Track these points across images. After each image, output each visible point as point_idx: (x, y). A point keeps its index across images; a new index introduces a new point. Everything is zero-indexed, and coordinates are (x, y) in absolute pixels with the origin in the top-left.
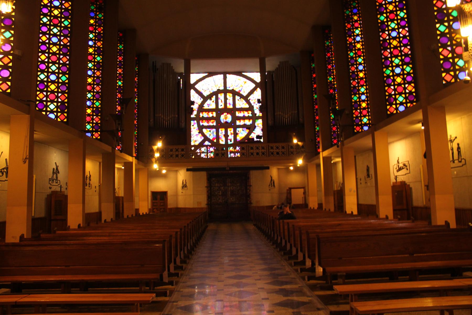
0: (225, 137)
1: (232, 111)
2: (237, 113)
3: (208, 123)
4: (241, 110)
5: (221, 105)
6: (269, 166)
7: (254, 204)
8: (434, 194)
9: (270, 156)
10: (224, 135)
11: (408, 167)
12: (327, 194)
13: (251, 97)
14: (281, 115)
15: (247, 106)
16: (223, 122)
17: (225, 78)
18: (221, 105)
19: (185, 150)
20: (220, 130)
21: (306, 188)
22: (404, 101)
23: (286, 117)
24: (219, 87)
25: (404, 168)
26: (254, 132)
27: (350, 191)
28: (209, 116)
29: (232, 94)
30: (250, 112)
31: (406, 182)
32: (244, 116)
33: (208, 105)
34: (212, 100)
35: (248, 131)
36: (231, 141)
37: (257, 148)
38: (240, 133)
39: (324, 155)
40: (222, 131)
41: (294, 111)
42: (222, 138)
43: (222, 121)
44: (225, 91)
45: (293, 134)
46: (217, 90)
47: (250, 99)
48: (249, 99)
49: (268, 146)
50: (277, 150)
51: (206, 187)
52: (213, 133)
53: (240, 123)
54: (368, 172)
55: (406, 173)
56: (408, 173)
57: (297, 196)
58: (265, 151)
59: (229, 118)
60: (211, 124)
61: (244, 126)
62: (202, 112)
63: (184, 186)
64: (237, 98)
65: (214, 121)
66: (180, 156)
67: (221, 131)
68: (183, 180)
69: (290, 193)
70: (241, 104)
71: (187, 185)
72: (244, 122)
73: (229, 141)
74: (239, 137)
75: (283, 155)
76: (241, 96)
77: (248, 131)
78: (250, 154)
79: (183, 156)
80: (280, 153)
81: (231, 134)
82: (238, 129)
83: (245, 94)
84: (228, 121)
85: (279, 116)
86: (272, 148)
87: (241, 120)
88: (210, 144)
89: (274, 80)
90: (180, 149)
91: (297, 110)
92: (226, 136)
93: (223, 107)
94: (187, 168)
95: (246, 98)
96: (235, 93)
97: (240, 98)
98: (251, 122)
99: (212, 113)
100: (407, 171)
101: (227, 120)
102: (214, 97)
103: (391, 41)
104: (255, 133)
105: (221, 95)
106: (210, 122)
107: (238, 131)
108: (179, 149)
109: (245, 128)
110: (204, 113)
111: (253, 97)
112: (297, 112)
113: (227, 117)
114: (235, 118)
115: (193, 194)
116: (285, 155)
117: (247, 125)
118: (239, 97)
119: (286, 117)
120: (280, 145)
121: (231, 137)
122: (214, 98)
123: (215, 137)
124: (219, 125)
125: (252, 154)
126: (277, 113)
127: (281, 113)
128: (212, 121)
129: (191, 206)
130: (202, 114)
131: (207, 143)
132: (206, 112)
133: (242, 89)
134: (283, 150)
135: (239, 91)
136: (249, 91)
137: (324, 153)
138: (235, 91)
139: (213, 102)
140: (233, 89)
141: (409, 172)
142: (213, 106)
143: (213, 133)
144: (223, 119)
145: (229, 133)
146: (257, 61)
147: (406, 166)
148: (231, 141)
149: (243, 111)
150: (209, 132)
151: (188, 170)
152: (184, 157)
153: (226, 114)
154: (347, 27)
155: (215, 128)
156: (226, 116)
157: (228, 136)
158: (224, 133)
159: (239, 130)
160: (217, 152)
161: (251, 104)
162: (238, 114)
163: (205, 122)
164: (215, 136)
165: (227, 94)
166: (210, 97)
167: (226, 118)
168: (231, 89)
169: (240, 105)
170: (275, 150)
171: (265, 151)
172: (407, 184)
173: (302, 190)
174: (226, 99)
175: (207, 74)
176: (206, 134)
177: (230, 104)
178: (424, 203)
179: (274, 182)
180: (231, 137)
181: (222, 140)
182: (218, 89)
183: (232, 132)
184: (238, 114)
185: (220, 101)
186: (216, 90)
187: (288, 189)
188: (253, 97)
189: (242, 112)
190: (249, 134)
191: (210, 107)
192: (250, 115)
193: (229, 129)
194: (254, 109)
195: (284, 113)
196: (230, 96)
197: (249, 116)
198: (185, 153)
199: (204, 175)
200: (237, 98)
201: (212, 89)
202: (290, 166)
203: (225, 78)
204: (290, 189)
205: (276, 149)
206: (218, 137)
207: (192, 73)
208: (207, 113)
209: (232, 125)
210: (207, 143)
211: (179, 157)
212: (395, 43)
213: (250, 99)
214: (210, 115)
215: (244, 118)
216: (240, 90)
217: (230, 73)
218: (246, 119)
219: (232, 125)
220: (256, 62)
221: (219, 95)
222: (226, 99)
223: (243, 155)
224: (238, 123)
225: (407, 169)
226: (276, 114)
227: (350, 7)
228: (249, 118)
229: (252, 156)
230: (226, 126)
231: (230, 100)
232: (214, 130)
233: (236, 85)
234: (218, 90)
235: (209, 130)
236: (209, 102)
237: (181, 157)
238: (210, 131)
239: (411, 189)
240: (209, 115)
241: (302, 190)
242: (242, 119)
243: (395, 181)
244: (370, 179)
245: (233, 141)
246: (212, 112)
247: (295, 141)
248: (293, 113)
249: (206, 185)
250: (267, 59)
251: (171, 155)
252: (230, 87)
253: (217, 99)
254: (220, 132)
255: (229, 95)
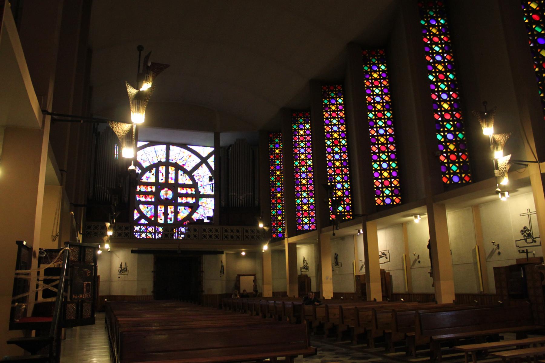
0: (164, 215)
1: (174, 187)
2: (179, 189)
3: (146, 198)
4: (184, 186)
5: (162, 180)
6: (223, 251)
7: (206, 292)
8: (439, 280)
9: (224, 239)
10: (164, 213)
11: (388, 256)
12: (291, 282)
13: (195, 173)
14: (235, 195)
15: (190, 182)
16: (163, 199)
17: (168, 150)
18: (162, 180)
19: (129, 229)
20: (159, 207)
21: (259, 276)
22: (390, 194)
23: (241, 199)
24: (161, 159)
25: (383, 257)
26: (197, 211)
27: (327, 279)
28: (147, 190)
29: (175, 168)
30: (193, 190)
31: (385, 270)
32: (187, 193)
33: (147, 177)
34: (152, 173)
35: (190, 210)
36: (171, 220)
37: (211, 230)
38: (181, 212)
39: (290, 242)
40: (162, 208)
41: (250, 193)
42: (161, 217)
43: (162, 198)
44: (167, 164)
45: (259, 218)
46: (159, 161)
47: (194, 175)
48: (193, 174)
49: (223, 228)
50: (232, 234)
51: (152, 272)
52: (151, 210)
53: (182, 201)
54: (337, 261)
55: (385, 261)
56: (388, 262)
57: (247, 284)
58: (219, 234)
59: (170, 195)
60: (149, 200)
61: (186, 205)
62: (140, 186)
63: (123, 270)
64: (180, 172)
65: (152, 196)
66: (123, 235)
67: (161, 208)
68: (122, 263)
69: (239, 281)
70: (184, 179)
71: (128, 269)
72: (187, 200)
73: (169, 220)
74: (181, 216)
75: (238, 239)
76: (185, 171)
77: (190, 210)
78: (202, 237)
79: (126, 235)
80: (235, 237)
81: (172, 212)
82: (179, 207)
83: (189, 169)
84: (168, 198)
85: (233, 197)
86: (226, 231)
87: (184, 198)
88: (146, 222)
89: (229, 157)
90: (123, 227)
91: (252, 191)
92: (166, 214)
93: (163, 181)
94: (131, 249)
95: (190, 173)
96: (178, 167)
97: (183, 173)
98: (194, 200)
99: (151, 188)
100: (387, 260)
101: (168, 196)
102: (154, 169)
103: (379, 138)
104: (198, 213)
105: (162, 167)
106: (148, 197)
107: (180, 210)
108: (98, 226)
109: (187, 206)
110: (142, 186)
111: (198, 173)
112: (252, 193)
113: (168, 193)
114: (177, 195)
115: (138, 280)
116: (240, 239)
117: (189, 203)
118: (182, 172)
119: (241, 199)
120: (235, 228)
121: (171, 216)
122: (154, 171)
123: (153, 215)
124: (159, 202)
125: (205, 236)
126: (231, 194)
127: (236, 194)
128: (150, 196)
129: (134, 294)
130: (140, 187)
131: (143, 221)
132: (144, 186)
133: (186, 163)
134: (238, 234)
135: (183, 166)
136: (194, 166)
137: (290, 239)
138: (178, 164)
139: (153, 175)
140: (176, 162)
141: (389, 261)
142: (153, 179)
143: (151, 210)
144: (163, 195)
145: (169, 212)
146: (212, 135)
147: (386, 255)
148: (171, 220)
149: (186, 188)
150: (147, 209)
151: (133, 252)
152: (128, 237)
153: (167, 189)
154: (325, 116)
155: (153, 205)
156: (166, 191)
157: (168, 214)
158: (163, 211)
159: (181, 208)
160: (167, 233)
161: (195, 181)
162: (180, 190)
163: (142, 197)
164: (153, 214)
165: (170, 167)
166: (149, 169)
167: (166, 194)
168: (174, 162)
169: (183, 181)
170: (229, 234)
171: (219, 234)
172: (386, 272)
173: (252, 277)
174: (167, 172)
175: (148, 143)
176: (142, 210)
177: (172, 179)
178: (407, 290)
179: (223, 268)
180: (171, 216)
181: (161, 219)
182: (159, 160)
183: (173, 210)
184: (180, 190)
185: (160, 174)
186: (157, 162)
187: (237, 276)
188: (198, 173)
189: (185, 189)
190: (191, 214)
191: (150, 181)
192: (194, 192)
193: (169, 207)
194: (198, 186)
195: (239, 194)
196: (173, 170)
197: (192, 193)
198: (129, 232)
199: (150, 258)
200: (180, 172)
201: (153, 161)
202: (242, 251)
203: (168, 150)
204: (239, 276)
205: (230, 233)
206: (156, 215)
207: (139, 141)
208: (145, 186)
209: (173, 202)
210: (143, 221)
211: (122, 237)
212: (382, 140)
213: (194, 175)
214: (149, 189)
215: (187, 195)
216: (184, 164)
217: (174, 144)
218: (189, 197)
219: (173, 202)
220: (211, 136)
221: (160, 168)
222: (167, 172)
223: (217, 238)
224: (180, 200)
225: (387, 258)
226: (229, 194)
227: (328, 97)
228: (192, 196)
229: (205, 239)
230: (166, 203)
231: (172, 173)
232: (153, 206)
233: (180, 158)
234: (160, 162)
235: (147, 206)
236: (148, 174)
237: (124, 237)
238: (147, 207)
239: (391, 276)
240: (147, 189)
241: (252, 277)
242: (185, 197)
243: (300, 274)
244: (339, 267)
245: (173, 220)
246: (151, 186)
247: (261, 225)
248: (248, 195)
249: (152, 269)
250: (221, 134)
251: (125, 235)
252: (172, 160)
253: (157, 172)
254: (159, 209)
255: (172, 169)
